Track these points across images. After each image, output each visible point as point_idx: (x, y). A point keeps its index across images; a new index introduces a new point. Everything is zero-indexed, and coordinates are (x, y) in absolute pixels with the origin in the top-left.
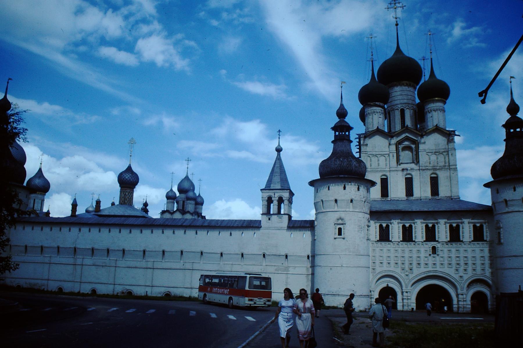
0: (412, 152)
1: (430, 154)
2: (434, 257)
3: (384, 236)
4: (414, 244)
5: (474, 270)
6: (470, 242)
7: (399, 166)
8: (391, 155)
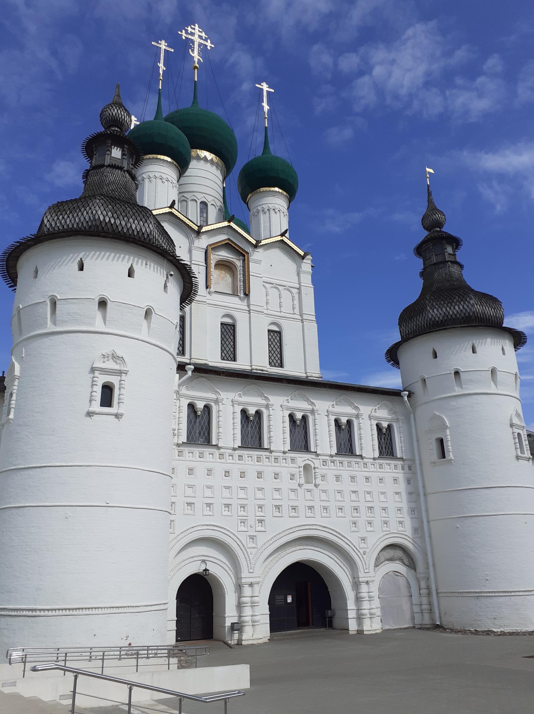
1: (268, 286)
2: (309, 491)
3: (200, 427)
6: (374, 459)
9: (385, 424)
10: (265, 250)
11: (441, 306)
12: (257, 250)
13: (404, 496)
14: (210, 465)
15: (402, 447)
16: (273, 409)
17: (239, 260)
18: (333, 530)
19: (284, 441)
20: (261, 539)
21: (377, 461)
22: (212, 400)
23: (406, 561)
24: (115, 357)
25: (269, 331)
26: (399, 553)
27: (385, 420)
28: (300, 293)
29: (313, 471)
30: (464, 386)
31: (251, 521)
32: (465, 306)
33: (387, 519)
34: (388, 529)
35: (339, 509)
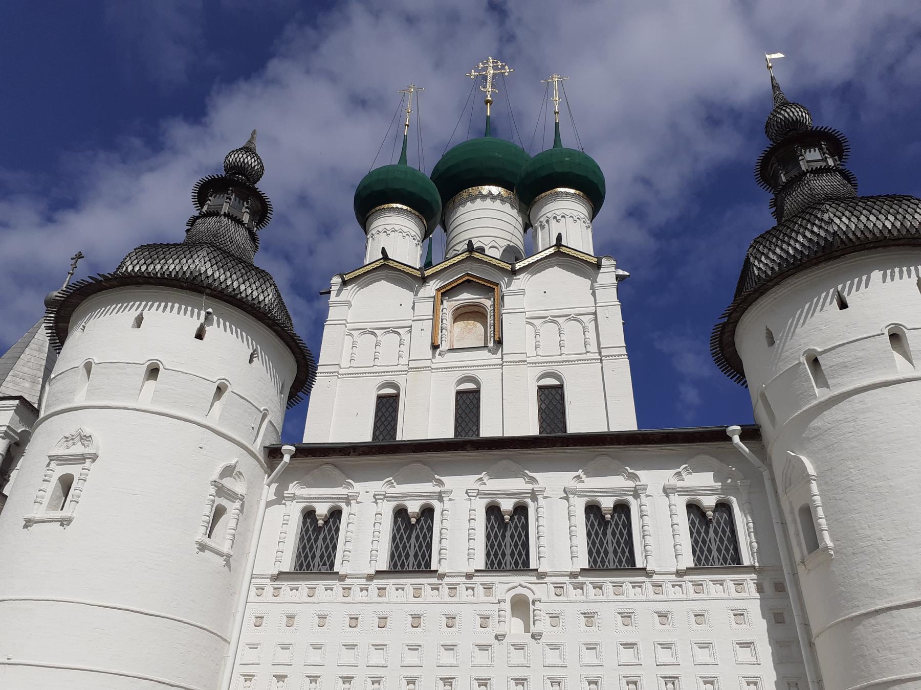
0: (485, 325)
1: (537, 322)
6: (679, 573)
8: (416, 326)
9: (709, 502)
11: (773, 247)
13: (765, 651)
14: (323, 609)
15: (751, 543)
16: (648, 496)
17: (489, 299)
19: (468, 554)
21: (686, 578)
22: (340, 499)
24: (85, 439)
25: (540, 388)
27: (709, 491)
28: (596, 320)
30: (830, 382)
32: (815, 229)
35: (590, 683)
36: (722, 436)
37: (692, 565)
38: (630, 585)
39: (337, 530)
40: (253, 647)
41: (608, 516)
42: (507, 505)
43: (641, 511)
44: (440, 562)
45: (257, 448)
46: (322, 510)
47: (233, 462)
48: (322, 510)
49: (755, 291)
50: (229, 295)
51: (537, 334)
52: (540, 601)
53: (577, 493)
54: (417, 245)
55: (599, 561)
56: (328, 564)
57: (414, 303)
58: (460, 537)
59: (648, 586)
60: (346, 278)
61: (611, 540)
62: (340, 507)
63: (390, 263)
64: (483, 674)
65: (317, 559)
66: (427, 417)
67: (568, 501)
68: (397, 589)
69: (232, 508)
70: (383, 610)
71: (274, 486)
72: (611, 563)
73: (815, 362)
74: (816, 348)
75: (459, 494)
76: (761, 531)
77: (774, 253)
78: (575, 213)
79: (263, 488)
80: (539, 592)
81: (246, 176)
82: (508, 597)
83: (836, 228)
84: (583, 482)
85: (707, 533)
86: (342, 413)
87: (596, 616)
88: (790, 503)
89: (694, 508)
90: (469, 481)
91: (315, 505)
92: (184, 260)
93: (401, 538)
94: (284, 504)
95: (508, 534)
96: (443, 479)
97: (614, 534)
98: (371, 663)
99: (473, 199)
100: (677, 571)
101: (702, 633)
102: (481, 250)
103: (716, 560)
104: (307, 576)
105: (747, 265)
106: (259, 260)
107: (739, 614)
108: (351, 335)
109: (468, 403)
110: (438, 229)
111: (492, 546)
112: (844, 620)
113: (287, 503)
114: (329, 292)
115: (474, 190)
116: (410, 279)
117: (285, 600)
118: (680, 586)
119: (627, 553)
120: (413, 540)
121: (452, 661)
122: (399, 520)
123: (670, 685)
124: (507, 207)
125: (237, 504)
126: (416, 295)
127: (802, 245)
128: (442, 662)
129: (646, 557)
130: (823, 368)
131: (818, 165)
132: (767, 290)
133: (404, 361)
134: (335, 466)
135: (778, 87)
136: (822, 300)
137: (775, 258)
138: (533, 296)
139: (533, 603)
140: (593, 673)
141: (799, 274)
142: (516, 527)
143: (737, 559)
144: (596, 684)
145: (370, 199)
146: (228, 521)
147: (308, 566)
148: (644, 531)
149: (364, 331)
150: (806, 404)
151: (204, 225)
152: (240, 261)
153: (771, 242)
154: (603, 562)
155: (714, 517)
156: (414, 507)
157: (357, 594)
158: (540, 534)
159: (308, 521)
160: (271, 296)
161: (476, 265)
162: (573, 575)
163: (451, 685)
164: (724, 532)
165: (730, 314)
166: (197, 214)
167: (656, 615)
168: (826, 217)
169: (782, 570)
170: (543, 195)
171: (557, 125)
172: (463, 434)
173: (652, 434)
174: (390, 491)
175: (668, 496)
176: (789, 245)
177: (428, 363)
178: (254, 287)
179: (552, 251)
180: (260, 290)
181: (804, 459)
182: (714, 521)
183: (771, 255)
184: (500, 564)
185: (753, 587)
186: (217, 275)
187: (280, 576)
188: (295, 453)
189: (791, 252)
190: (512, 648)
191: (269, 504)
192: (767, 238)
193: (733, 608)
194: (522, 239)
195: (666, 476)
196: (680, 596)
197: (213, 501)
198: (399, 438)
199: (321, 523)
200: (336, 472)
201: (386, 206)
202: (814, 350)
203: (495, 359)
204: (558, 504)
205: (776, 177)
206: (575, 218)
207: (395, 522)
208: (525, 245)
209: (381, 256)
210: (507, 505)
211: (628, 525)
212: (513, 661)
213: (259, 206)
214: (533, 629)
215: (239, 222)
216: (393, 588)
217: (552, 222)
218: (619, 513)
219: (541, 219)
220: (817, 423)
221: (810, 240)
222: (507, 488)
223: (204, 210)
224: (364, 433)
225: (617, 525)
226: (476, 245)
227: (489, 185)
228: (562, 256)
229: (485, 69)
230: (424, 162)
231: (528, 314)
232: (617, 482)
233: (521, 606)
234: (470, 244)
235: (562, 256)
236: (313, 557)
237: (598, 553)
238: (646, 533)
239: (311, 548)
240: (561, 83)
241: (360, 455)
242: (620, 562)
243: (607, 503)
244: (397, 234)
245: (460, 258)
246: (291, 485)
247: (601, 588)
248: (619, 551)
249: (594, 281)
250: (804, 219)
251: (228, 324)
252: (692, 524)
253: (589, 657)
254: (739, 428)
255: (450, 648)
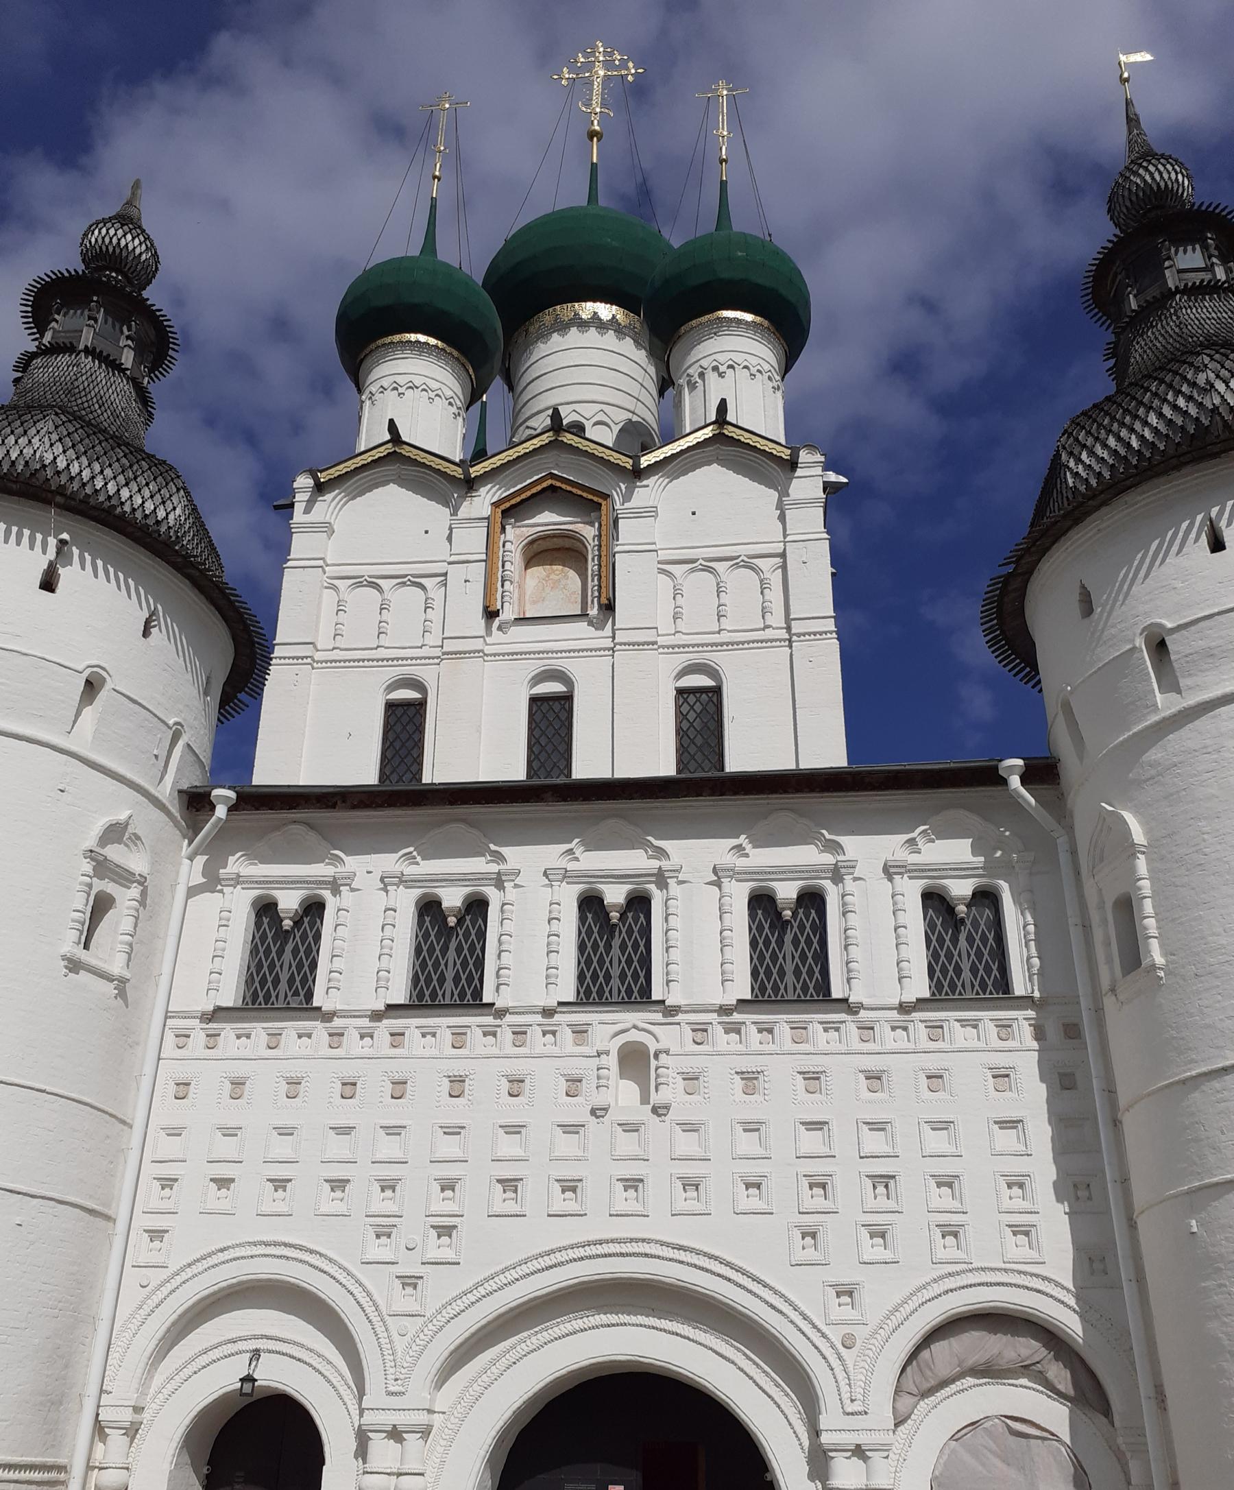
1: (677, 570)
4: (490, 1033)
5: (950, 1232)
6: (903, 1008)
7: (497, 635)
9: (961, 889)
10: (674, 476)
12: (645, 483)
13: (1041, 1133)
15: (1029, 958)
16: (516, 886)
17: (591, 524)
18: (716, 1258)
19: (547, 977)
20: (439, 1288)
21: (916, 1015)
22: (321, 883)
23: (1060, 1374)
25: (681, 692)
26: (1028, 1348)
27: (961, 871)
28: (784, 567)
29: (653, 1063)
30: (1183, 682)
31: (414, 1228)
32: (1181, 402)
33: (955, 1219)
34: (960, 1255)
36: (991, 777)
37: (927, 994)
38: (820, 1027)
39: (318, 937)
40: (175, 1132)
41: (787, 914)
42: (615, 895)
43: (844, 904)
44: (497, 991)
45: (166, 790)
46: (289, 901)
47: (122, 816)
48: (289, 901)
49: (1064, 517)
50: (98, 507)
51: (677, 592)
52: (667, 1052)
53: (734, 874)
54: (456, 416)
55: (769, 987)
56: (302, 993)
57: (451, 529)
58: (532, 945)
59: (851, 1029)
60: (323, 477)
61: (791, 953)
62: (646, 891)
63: (405, 451)
64: (569, 1172)
65: (283, 986)
66: (478, 743)
67: (720, 887)
68: (424, 1035)
69: (126, 897)
70: (399, 1069)
71: (201, 860)
72: (790, 989)
73: (1159, 647)
74: (1164, 622)
75: (531, 877)
76: (1048, 939)
77: (1105, 446)
78: (753, 361)
79: (180, 864)
80: (667, 1038)
81: (125, 275)
82: (615, 1046)
83: (1217, 401)
84: (747, 855)
85: (955, 941)
86: (315, 733)
87: (761, 1076)
88: (1100, 890)
89: (935, 900)
90: (550, 854)
91: (774, 885)
92: (12, 439)
93: (431, 950)
94: (221, 891)
95: (616, 943)
96: (505, 851)
97: (796, 942)
98: (379, 1156)
99: (562, 327)
100: (901, 1004)
101: (938, 1106)
102: (578, 429)
103: (968, 986)
104: (263, 1014)
105: (1056, 467)
106: (165, 434)
107: (1002, 1075)
108: (334, 588)
109: (551, 718)
110: (498, 383)
111: (589, 962)
112: (1172, 1084)
113: (225, 889)
114: (292, 505)
115: (564, 311)
116: (446, 482)
117: (227, 1055)
118: (905, 1029)
119: (817, 974)
120: (452, 953)
121: (518, 1152)
122: (427, 919)
123: (881, 1189)
124: (627, 345)
125: (135, 891)
126: (455, 513)
127: (1156, 431)
128: (500, 1154)
129: (849, 980)
130: (1173, 657)
131: (1197, 278)
132: (1088, 514)
133: (433, 639)
134: (464, 821)
135: (1138, 121)
136: (1181, 534)
137: (1106, 455)
138: (678, 519)
139: (656, 1056)
140: (753, 1169)
141: (1144, 487)
142: (630, 932)
143: (1004, 984)
144: (759, 1188)
145: (372, 319)
146: (118, 922)
147: (267, 998)
148: (847, 938)
149: (360, 582)
150: (1140, 721)
151: (43, 371)
152: (118, 441)
153: (1100, 425)
154: (776, 989)
155: (968, 914)
156: (452, 898)
157: (353, 1044)
158: (671, 943)
159: (266, 920)
160: (178, 511)
161: (565, 457)
162: (724, 1010)
163: (516, 1191)
164: (984, 939)
165: (1020, 558)
166: (32, 347)
167: (862, 1076)
168: (1201, 379)
169: (1078, 1003)
170: (694, 323)
171: (723, 185)
172: (542, 772)
173: (870, 773)
174: (410, 870)
175: (890, 879)
176: (1132, 430)
177: (477, 644)
178: (147, 493)
179: (708, 433)
180: (158, 498)
181: (1129, 817)
182: (968, 923)
183: (1099, 450)
184: (600, 993)
185: (1027, 1031)
186: (75, 469)
187: (218, 1014)
188: (234, 802)
189: (1135, 443)
190: (619, 1129)
191: (192, 892)
192: (1092, 418)
193: (993, 1066)
194: (654, 410)
195: (890, 846)
196: (904, 1045)
197: (90, 886)
198: (426, 779)
199: (287, 924)
200: (312, 836)
201: (396, 338)
202: (1161, 626)
203: (600, 638)
204: (702, 894)
205: (1120, 299)
206: (754, 370)
207: (420, 923)
208: (660, 421)
209: (388, 437)
210: (615, 895)
211: (821, 928)
212: (621, 1151)
213: (152, 333)
214: (655, 1098)
215: (114, 365)
216: (418, 1033)
217: (711, 377)
218: (807, 908)
219: (690, 371)
220: (1154, 754)
221: (1170, 423)
222: (615, 866)
223: (48, 337)
224: (361, 767)
225: (802, 927)
226: (568, 417)
227: (594, 300)
228: (727, 445)
229: (589, 66)
230: (470, 252)
231: (663, 555)
232: (806, 855)
233: (635, 1061)
234: (556, 416)
235: (727, 445)
236: (276, 981)
237: (768, 973)
238: (850, 941)
239: (272, 967)
240: (732, 99)
241: (354, 807)
242: (805, 989)
243: (787, 892)
244: (416, 394)
245: (537, 443)
246: (231, 859)
247: (770, 1031)
248: (804, 971)
249: (784, 493)
250: (1162, 381)
251: (100, 563)
252: (930, 926)
253: (747, 1144)
254: (1020, 762)
255: (513, 1130)
